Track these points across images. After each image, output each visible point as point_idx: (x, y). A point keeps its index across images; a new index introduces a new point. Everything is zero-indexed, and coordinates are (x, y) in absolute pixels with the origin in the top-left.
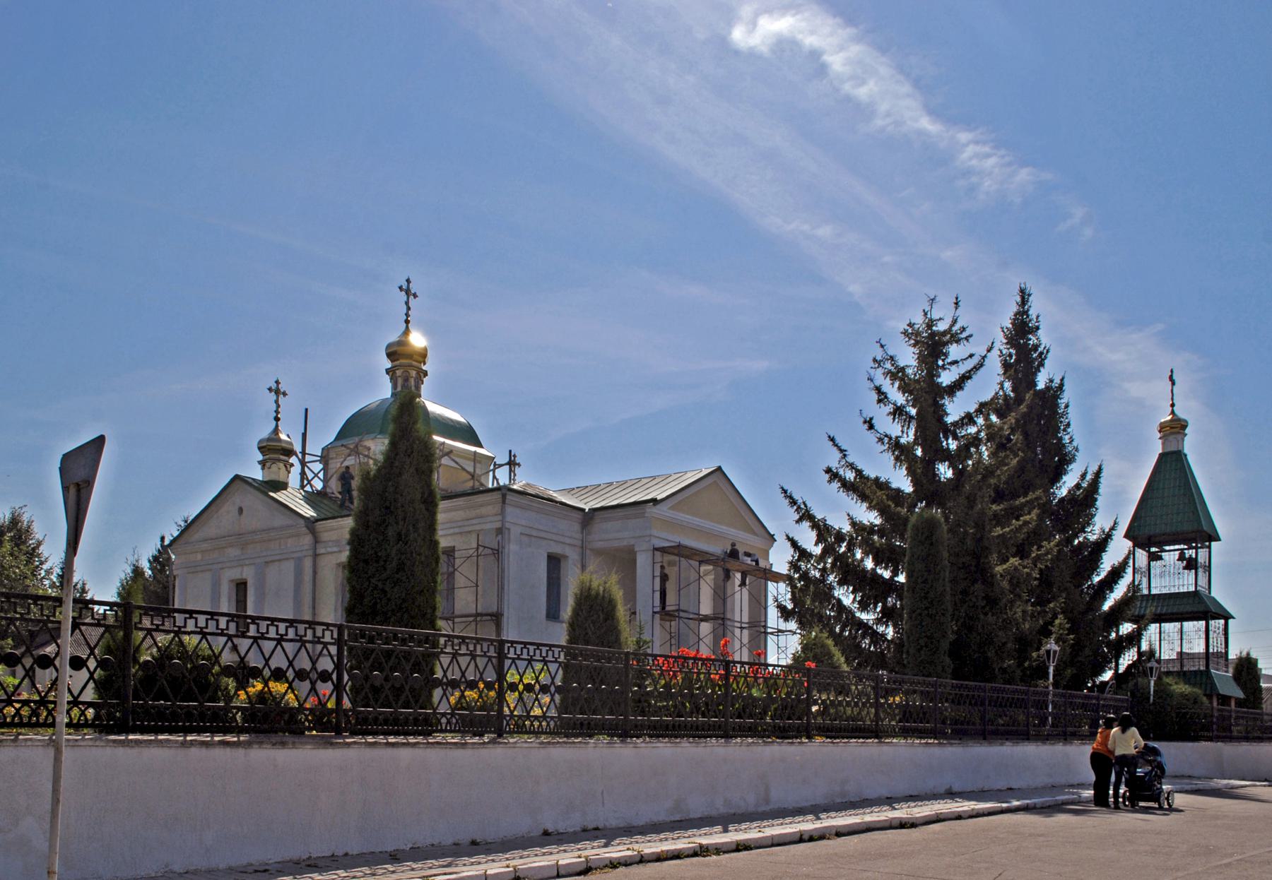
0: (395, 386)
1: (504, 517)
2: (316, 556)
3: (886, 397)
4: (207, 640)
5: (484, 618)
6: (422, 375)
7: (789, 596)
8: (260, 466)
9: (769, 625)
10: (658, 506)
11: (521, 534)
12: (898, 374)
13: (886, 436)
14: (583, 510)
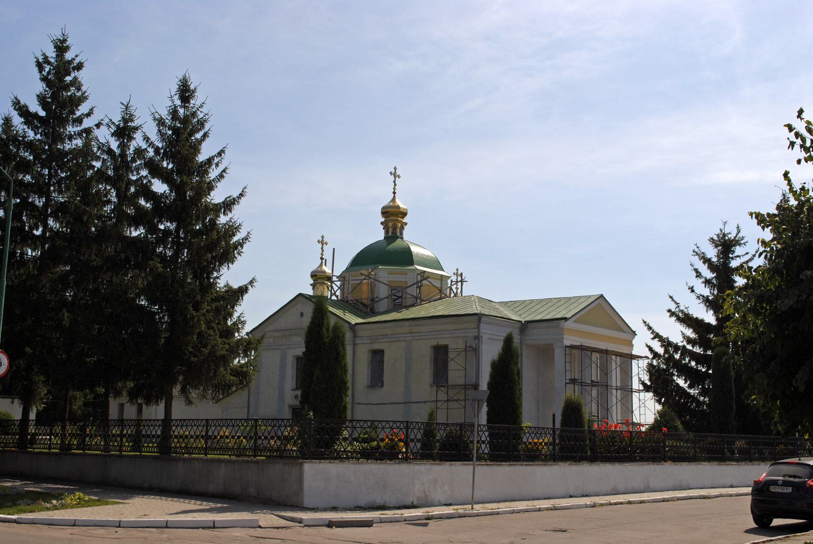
0: (387, 232)
1: (479, 330)
2: (354, 345)
3: (700, 275)
5: (470, 387)
6: (404, 225)
8: (311, 287)
9: (633, 388)
10: (568, 322)
12: (706, 260)
13: (701, 295)
14: (521, 322)
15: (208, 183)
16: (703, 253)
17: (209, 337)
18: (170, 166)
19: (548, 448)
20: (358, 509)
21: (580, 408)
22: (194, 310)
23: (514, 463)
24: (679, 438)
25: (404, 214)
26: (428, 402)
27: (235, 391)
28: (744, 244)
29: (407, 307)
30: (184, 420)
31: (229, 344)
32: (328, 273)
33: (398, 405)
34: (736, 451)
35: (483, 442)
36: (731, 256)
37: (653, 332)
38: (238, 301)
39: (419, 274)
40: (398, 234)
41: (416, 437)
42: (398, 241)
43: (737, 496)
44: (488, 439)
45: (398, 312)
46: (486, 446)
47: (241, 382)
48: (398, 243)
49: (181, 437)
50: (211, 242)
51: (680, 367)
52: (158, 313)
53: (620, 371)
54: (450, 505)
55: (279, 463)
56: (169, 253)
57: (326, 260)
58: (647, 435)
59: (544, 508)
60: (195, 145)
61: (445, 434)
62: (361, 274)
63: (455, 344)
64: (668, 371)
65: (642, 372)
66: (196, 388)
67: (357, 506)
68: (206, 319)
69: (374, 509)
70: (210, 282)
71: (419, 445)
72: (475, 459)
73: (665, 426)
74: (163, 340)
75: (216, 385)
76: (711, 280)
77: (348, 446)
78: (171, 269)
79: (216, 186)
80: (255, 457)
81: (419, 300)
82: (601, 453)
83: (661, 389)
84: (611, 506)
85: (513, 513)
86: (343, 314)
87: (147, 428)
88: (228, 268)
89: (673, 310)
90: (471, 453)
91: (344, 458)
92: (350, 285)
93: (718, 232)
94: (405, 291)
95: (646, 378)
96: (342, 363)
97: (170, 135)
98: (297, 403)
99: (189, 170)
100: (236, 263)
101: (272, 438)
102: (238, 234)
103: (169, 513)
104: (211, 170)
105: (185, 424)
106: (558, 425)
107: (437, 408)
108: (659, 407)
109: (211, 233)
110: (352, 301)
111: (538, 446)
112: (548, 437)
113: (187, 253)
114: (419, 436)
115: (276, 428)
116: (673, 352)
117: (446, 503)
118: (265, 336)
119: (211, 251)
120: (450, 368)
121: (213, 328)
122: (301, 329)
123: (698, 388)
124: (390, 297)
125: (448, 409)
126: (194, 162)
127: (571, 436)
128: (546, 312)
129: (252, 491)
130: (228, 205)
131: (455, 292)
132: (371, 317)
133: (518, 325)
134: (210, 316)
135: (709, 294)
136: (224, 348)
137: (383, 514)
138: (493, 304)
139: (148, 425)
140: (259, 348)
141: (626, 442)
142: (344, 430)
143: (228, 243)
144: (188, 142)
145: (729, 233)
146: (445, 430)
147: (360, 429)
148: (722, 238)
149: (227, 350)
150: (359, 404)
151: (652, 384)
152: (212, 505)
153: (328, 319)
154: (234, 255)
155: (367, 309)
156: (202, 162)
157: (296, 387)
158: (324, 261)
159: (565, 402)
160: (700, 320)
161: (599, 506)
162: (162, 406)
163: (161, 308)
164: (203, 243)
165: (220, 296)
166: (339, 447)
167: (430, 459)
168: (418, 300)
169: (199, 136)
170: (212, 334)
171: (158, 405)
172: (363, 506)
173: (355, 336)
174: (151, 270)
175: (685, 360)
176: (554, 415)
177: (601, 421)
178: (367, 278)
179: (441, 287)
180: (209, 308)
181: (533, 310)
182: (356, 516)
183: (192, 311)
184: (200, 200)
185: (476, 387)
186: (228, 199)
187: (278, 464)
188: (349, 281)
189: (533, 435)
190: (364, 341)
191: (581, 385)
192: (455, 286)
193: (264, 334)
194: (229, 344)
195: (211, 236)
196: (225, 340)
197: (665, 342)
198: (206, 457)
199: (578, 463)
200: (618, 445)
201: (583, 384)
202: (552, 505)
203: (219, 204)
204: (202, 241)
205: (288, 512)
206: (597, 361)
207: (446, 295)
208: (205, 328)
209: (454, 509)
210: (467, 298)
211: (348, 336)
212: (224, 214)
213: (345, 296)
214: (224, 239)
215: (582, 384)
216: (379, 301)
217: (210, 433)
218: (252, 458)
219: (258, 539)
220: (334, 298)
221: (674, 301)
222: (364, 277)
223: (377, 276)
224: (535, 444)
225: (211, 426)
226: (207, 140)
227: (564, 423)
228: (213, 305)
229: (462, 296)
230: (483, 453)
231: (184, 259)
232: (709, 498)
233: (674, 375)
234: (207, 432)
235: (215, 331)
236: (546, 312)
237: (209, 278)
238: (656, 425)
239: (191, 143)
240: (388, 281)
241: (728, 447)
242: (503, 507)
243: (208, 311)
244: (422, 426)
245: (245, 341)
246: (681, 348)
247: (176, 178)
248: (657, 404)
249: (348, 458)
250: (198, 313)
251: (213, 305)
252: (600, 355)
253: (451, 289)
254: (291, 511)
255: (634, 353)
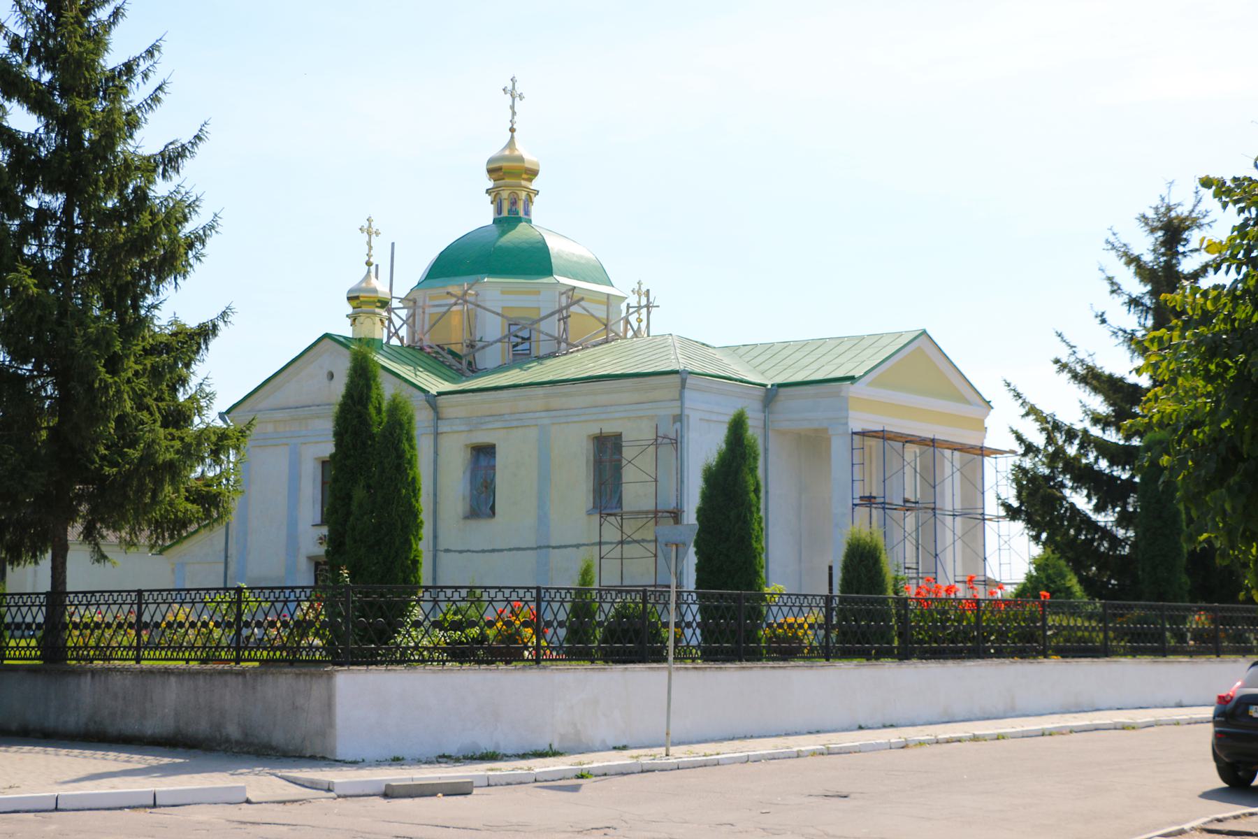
0: (499, 210)
1: (682, 403)
2: (437, 434)
3: (1119, 288)
4: (430, 601)
6: (532, 195)
7: (1014, 492)
8: (349, 321)
9: (986, 512)
10: (857, 385)
11: (701, 419)
12: (1133, 260)
13: (1121, 330)
14: (765, 386)
15: (128, 114)
16: (1125, 245)
17: (141, 427)
18: (47, 77)
19: (816, 634)
20: (445, 760)
21: (878, 554)
22: (107, 372)
23: (749, 664)
24: (1074, 611)
25: (532, 173)
26: (584, 545)
27: (196, 532)
28: (1208, 224)
29: (540, 359)
30: (93, 593)
31: (182, 439)
32: (383, 293)
33: (524, 552)
34: (1189, 635)
35: (689, 625)
36: (1181, 249)
37: (1024, 403)
38: (197, 352)
39: (563, 294)
40: (521, 214)
41: (555, 618)
42: (522, 227)
43: (1189, 724)
44: (698, 618)
45: (522, 369)
46: (694, 633)
47: (208, 514)
48: (519, 234)
49: (87, 626)
50: (139, 235)
51: (1076, 472)
52: (32, 378)
53: (962, 480)
54: (624, 748)
55: (286, 674)
56: (50, 256)
57: (377, 266)
58: (1009, 607)
59: (807, 751)
60: (96, 33)
61: (613, 610)
62: (448, 293)
63: (635, 431)
64: (1053, 478)
65: (1004, 482)
66: (116, 528)
67: (441, 754)
68: (133, 389)
69: (475, 759)
70: (139, 315)
71: (562, 632)
72: (671, 657)
73: (1047, 589)
74: (44, 434)
75: (157, 521)
76: (1140, 298)
77: (422, 638)
78: (57, 290)
79: (145, 119)
80: (237, 663)
81: (563, 345)
82: (921, 642)
83: (1040, 515)
84: (938, 746)
85: (748, 761)
86: (414, 376)
87: (14, 610)
88: (176, 287)
89: (1064, 360)
90: (665, 647)
91: (415, 661)
92: (427, 317)
93: (1156, 202)
94: (536, 326)
95: (1011, 495)
96: (408, 475)
97: (41, 11)
98: (321, 550)
99: (87, 87)
100: (192, 276)
101: (272, 624)
102: (194, 216)
103: (62, 780)
104: (134, 87)
105: (93, 601)
106: (837, 591)
107: (601, 558)
108: (1037, 550)
109: (138, 216)
110: (431, 347)
111: (796, 630)
112: (816, 612)
113: (90, 256)
114: (562, 616)
115: (279, 606)
116: (1065, 442)
117: (617, 745)
118: (254, 422)
119: (140, 254)
120: (625, 479)
121: (148, 408)
122: (329, 404)
123: (1114, 512)
124: (507, 340)
125: (622, 559)
126: (96, 68)
127: (861, 610)
128: (815, 366)
129: (233, 731)
130: (171, 159)
131: (635, 328)
132: (468, 378)
133: (760, 392)
134: (142, 384)
135: (1136, 327)
136: (172, 447)
137: (492, 770)
138: (710, 350)
139: (16, 605)
140: (242, 446)
141: (968, 619)
142: (415, 606)
143: (174, 240)
144: (81, 26)
145: (1179, 205)
146: (613, 603)
147: (446, 603)
148: (1165, 215)
149: (178, 452)
150: (447, 551)
151: (1022, 504)
152: (151, 760)
153: (378, 389)
154: (187, 261)
155: (461, 363)
156: (113, 70)
157: (322, 521)
158: (373, 268)
159: (848, 543)
160: (1117, 379)
161: (916, 745)
162: (46, 561)
163: (37, 366)
164: (121, 236)
165: (161, 343)
166: (405, 640)
167: (584, 660)
168: (561, 346)
169: (103, 14)
170: (145, 420)
171: (36, 563)
172: (453, 754)
173: (438, 418)
174: (14, 291)
175: (1086, 456)
176: (831, 568)
177: (922, 578)
178: (460, 301)
179: (608, 319)
180: (139, 367)
181: (789, 362)
182: (440, 775)
183: (102, 374)
184: (111, 147)
185: (676, 516)
186: (171, 147)
187: (284, 676)
188: (424, 309)
189: (785, 609)
190: (455, 428)
191: (884, 508)
192: (636, 315)
193: (253, 419)
194: (182, 439)
195: (138, 224)
196: (174, 431)
197: (1048, 422)
198: (138, 666)
199: (874, 662)
200: (952, 625)
201: (887, 506)
202: (824, 745)
203: (153, 156)
204: (120, 232)
205: (304, 770)
206: (916, 460)
207: (617, 334)
208: (132, 408)
209: (632, 757)
210: (659, 339)
211: (421, 419)
212: (164, 176)
213: (416, 339)
214: (166, 229)
215: (884, 506)
216: (483, 348)
217: (146, 618)
218: (233, 664)
219: (243, 826)
220: (395, 342)
221: (1065, 341)
222: (453, 300)
223: (479, 298)
224: (790, 626)
225: (147, 604)
226: (122, 22)
227: (847, 585)
228: (146, 362)
229: (648, 336)
230: (688, 646)
231: (84, 269)
232: (1134, 728)
233: (1064, 486)
234: (140, 615)
235: (151, 414)
236: (815, 366)
237: (136, 307)
238: (1028, 585)
239: (89, 29)
240: (503, 308)
241: (1172, 628)
242: (728, 750)
243: (136, 374)
244: (568, 595)
245: (214, 433)
246: (1080, 434)
247: (59, 102)
248: (1032, 544)
249: (423, 661)
250: (116, 379)
251: (146, 362)
252: (920, 449)
253: (627, 322)
254: (311, 768)
255: (989, 443)
